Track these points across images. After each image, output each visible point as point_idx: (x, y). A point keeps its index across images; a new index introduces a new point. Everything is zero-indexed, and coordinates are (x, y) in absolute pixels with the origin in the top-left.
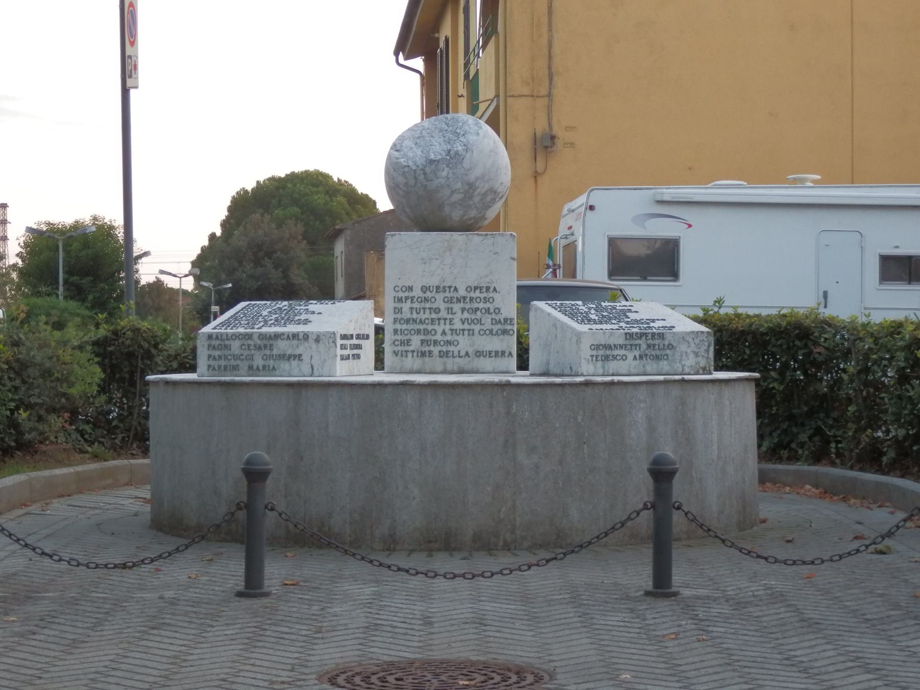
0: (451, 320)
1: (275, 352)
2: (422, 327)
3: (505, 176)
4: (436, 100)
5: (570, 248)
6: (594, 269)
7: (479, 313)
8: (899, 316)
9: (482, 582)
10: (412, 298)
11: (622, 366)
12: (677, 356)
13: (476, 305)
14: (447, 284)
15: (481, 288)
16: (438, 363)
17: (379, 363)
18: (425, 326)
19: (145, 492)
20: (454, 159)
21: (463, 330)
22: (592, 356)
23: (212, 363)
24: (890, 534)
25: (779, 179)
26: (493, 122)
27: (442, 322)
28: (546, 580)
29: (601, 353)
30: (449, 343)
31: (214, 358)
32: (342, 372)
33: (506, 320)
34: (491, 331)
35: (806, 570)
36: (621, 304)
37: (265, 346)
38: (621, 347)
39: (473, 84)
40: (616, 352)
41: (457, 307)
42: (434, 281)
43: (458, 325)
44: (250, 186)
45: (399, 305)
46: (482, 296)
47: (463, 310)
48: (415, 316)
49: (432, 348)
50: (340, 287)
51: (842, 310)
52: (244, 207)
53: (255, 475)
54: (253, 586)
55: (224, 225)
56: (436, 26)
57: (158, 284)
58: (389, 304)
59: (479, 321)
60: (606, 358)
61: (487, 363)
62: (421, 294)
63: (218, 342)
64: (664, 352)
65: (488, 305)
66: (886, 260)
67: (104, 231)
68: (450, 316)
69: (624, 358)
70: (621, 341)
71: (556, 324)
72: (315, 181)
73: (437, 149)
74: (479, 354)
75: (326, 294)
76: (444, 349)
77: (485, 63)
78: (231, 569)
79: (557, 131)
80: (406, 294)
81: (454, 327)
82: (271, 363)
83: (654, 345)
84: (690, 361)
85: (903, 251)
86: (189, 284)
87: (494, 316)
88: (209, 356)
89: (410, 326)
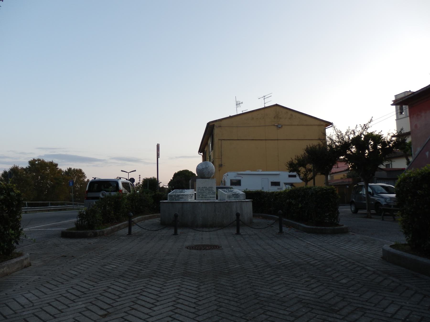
4: (204, 159)
5: (225, 181)
6: (228, 184)
8: (273, 191)
9: (211, 232)
11: (232, 199)
16: (204, 199)
17: (195, 199)
19: (160, 219)
20: (206, 168)
24: (273, 224)
25: (256, 171)
26: (213, 163)
28: (220, 232)
32: (190, 200)
35: (260, 230)
36: (232, 190)
39: (210, 157)
42: (203, 186)
44: (177, 172)
50: (190, 187)
51: (265, 190)
52: (176, 175)
54: (176, 233)
55: (173, 178)
58: (197, 190)
61: (212, 199)
63: (171, 196)
67: (154, 179)
71: (222, 193)
73: (204, 167)
75: (188, 188)
77: (211, 153)
78: (172, 231)
79: (223, 164)
84: (242, 198)
85: (274, 181)
86: (167, 187)
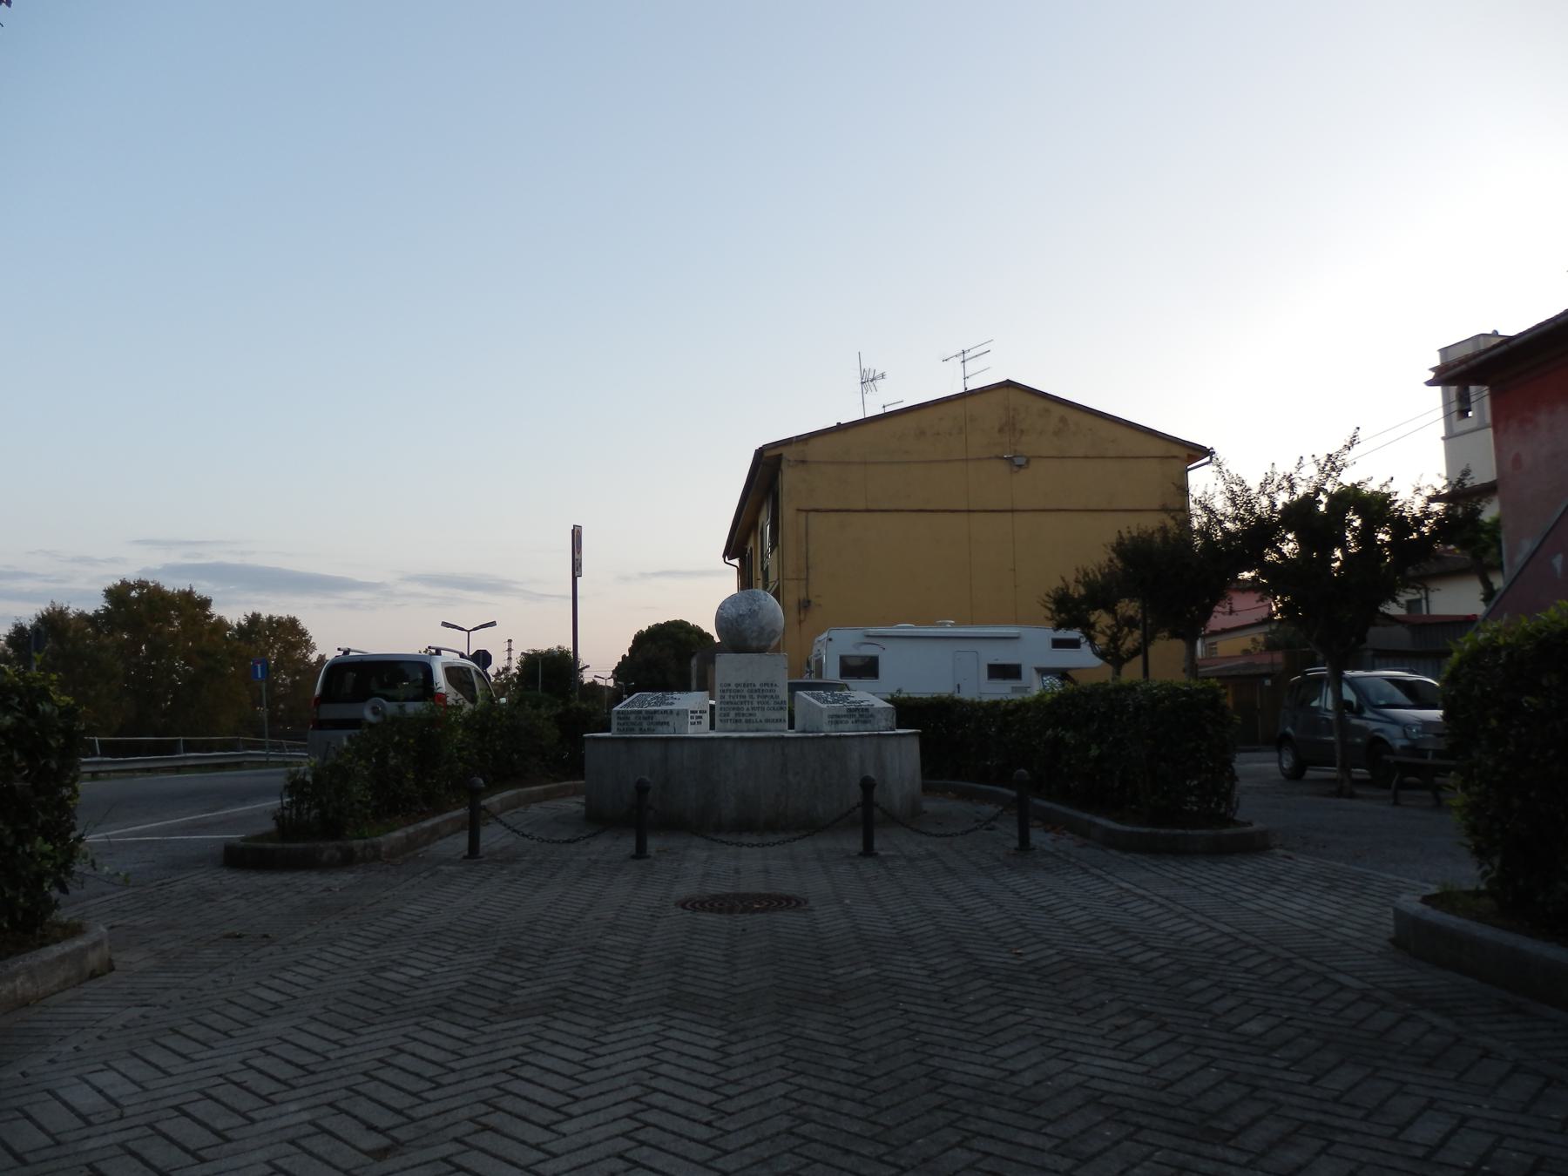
3: (782, 623)
4: (746, 580)
5: (819, 662)
6: (832, 673)
8: (997, 698)
11: (846, 727)
16: (745, 726)
17: (712, 727)
19: (582, 800)
20: (753, 614)
26: (776, 595)
28: (804, 847)
32: (691, 732)
39: (765, 573)
42: (742, 681)
50: (694, 683)
52: (641, 640)
53: (642, 789)
54: (640, 853)
55: (630, 650)
56: (746, 542)
57: (594, 683)
63: (623, 715)
66: (990, 666)
71: (809, 703)
72: (680, 626)
73: (744, 609)
74: (767, 721)
75: (686, 688)
77: (771, 560)
78: (628, 844)
84: (883, 723)
86: (611, 683)
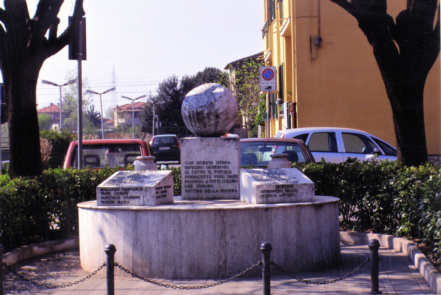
0: (210, 176)
1: (129, 195)
2: (197, 179)
7: (222, 173)
10: (193, 167)
12: (299, 194)
13: (221, 170)
14: (208, 160)
15: (223, 162)
18: (199, 179)
21: (215, 180)
22: (261, 196)
23: (103, 200)
27: (206, 177)
29: (265, 194)
30: (209, 186)
31: (104, 198)
33: (234, 176)
34: (228, 181)
37: (125, 193)
38: (274, 191)
40: (272, 194)
41: (212, 170)
42: (203, 159)
43: (213, 178)
45: (187, 170)
46: (223, 165)
47: (215, 172)
48: (194, 174)
49: (202, 188)
59: (222, 177)
60: (268, 196)
62: (197, 165)
64: (293, 193)
65: (226, 169)
68: (210, 174)
69: (275, 196)
70: (274, 189)
74: (223, 191)
76: (207, 189)
80: (190, 165)
81: (212, 179)
82: (127, 200)
83: (288, 190)
87: (228, 174)
88: (102, 197)
89: (192, 179)
